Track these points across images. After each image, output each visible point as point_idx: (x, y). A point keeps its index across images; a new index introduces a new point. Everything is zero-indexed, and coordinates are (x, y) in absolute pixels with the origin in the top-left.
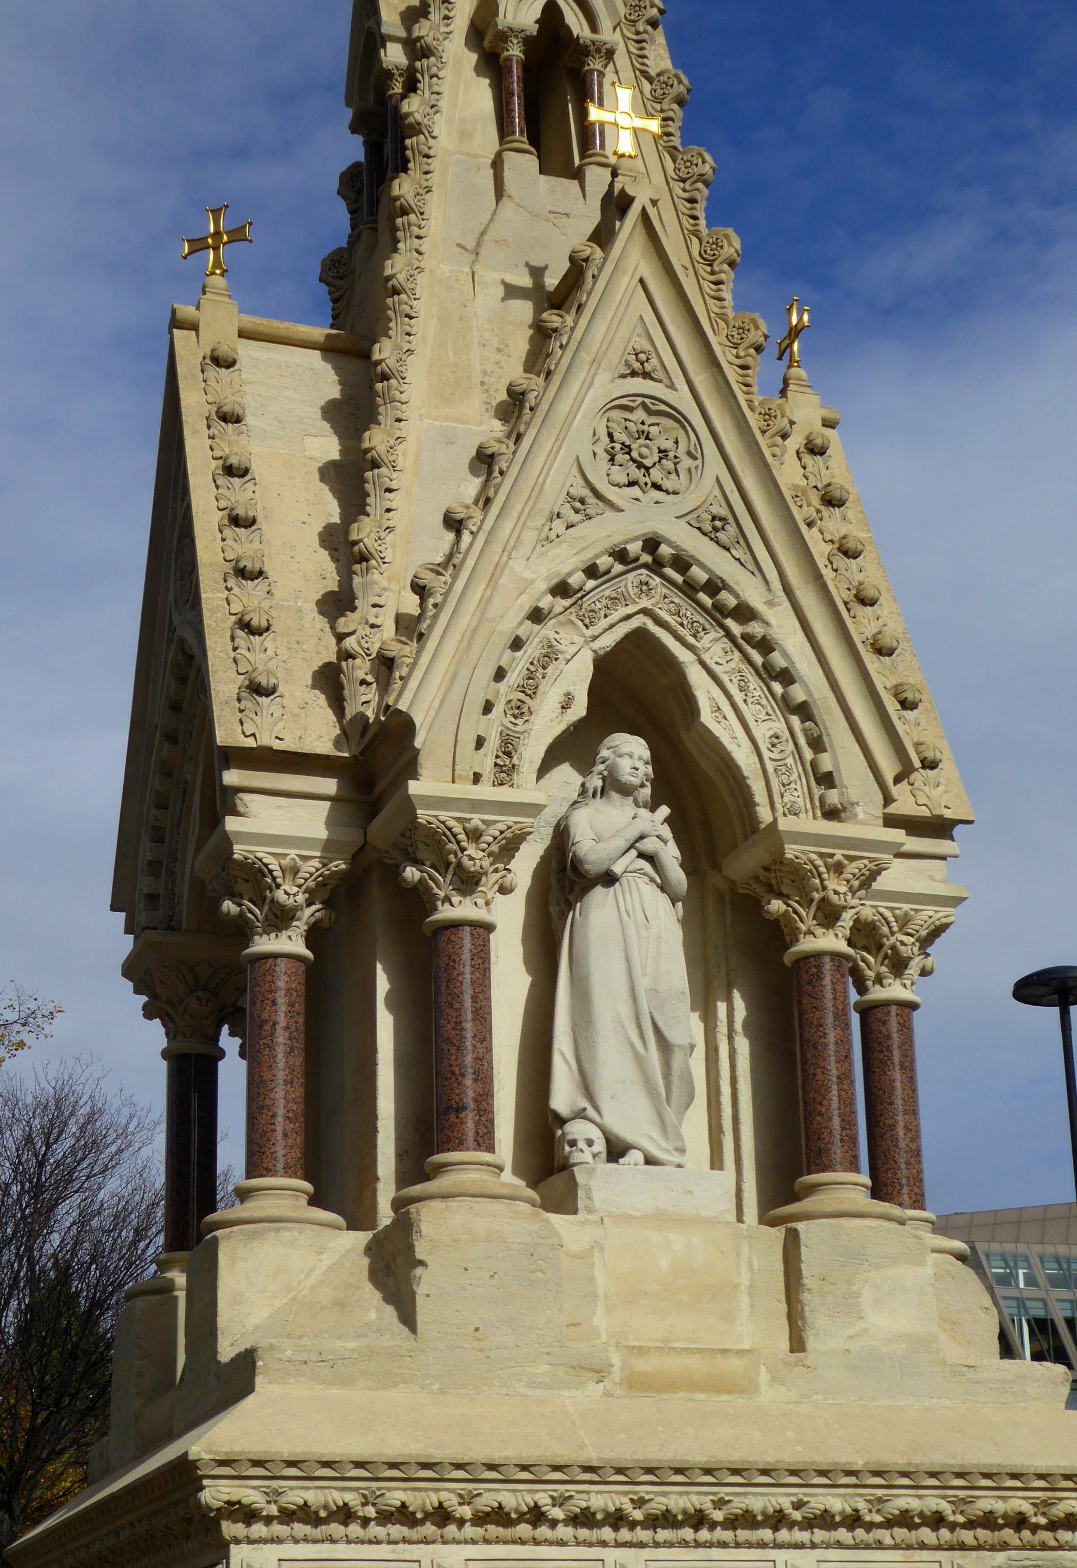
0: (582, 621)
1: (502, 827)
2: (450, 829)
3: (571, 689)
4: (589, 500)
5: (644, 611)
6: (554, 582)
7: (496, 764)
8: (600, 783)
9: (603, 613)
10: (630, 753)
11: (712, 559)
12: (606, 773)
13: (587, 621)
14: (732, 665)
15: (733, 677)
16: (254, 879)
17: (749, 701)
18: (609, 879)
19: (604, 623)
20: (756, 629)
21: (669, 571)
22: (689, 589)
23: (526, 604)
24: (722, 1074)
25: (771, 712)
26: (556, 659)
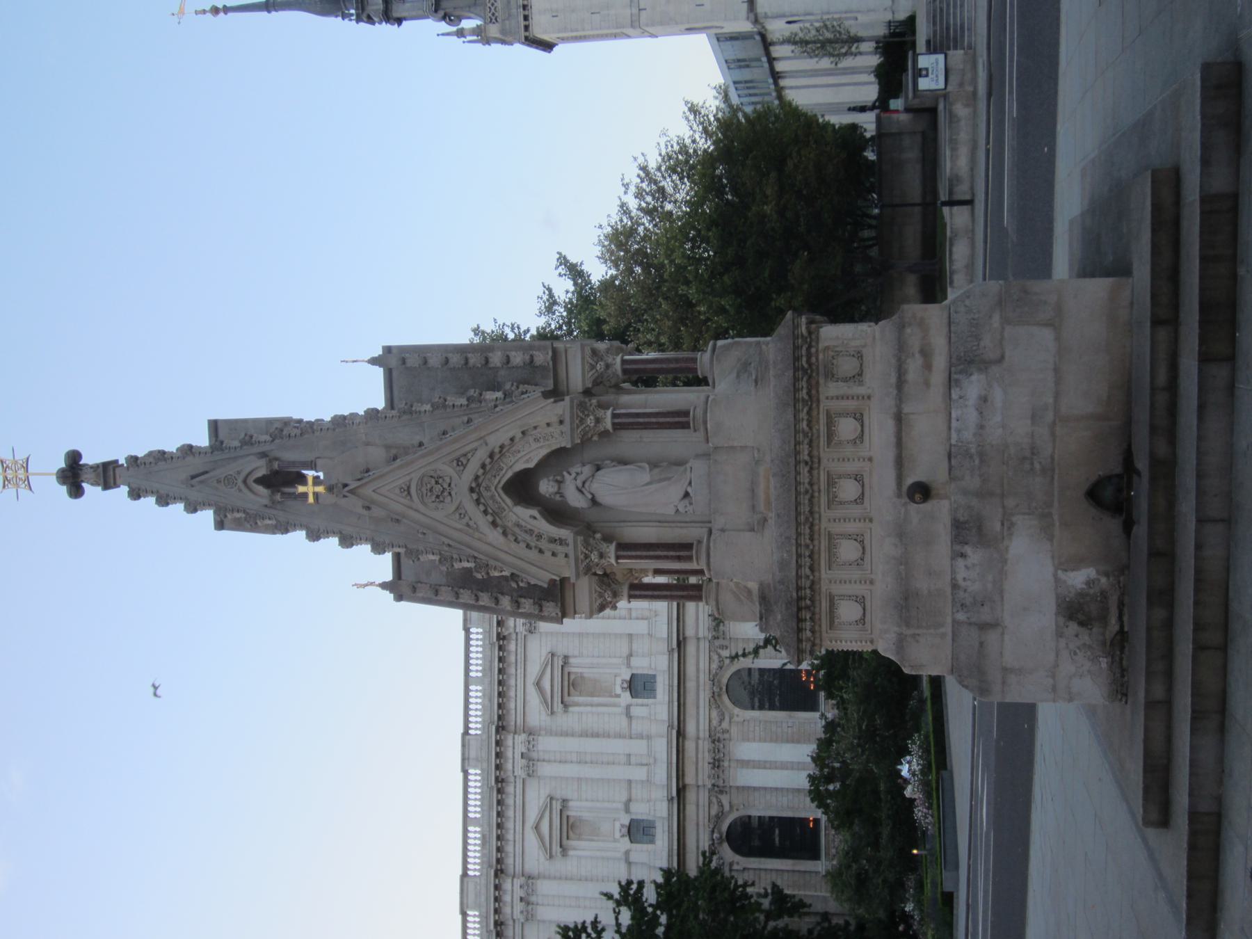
4: (460, 512)
11: (473, 467)
20: (497, 450)
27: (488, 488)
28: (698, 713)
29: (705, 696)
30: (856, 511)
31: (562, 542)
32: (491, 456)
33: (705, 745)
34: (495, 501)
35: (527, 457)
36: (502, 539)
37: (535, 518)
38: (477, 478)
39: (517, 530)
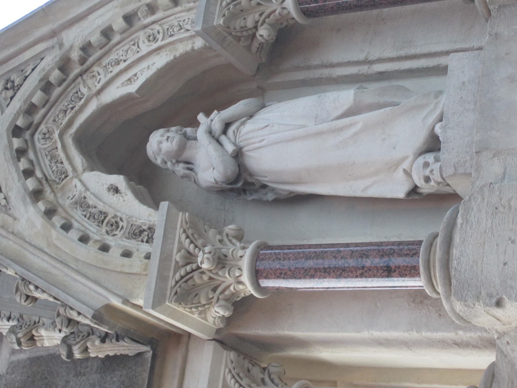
0: (63, 180)
1: (183, 236)
2: (182, 277)
3: (106, 186)
5: (61, 136)
6: (28, 200)
7: (147, 242)
8: (181, 165)
9: (60, 165)
10: (160, 144)
12: (174, 161)
13: (63, 176)
14: (101, 71)
15: (109, 70)
17: (124, 58)
18: (238, 155)
19: (67, 165)
20: (75, 55)
21: (37, 118)
24: (396, 68)
25: (132, 43)
26: (85, 198)
27: (47, 136)
32: (64, 66)
34: (53, 158)
36: (39, 221)
37: (116, 190)
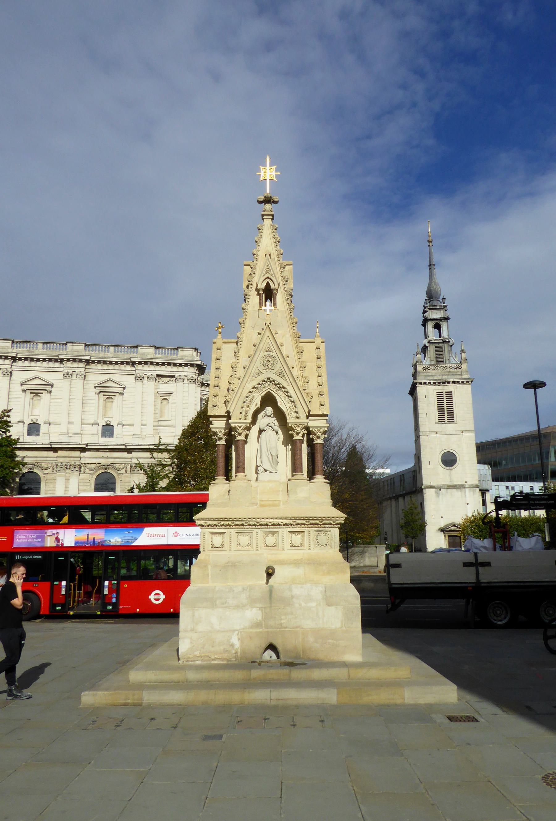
4: (259, 373)
11: (278, 379)
16: (215, 434)
22: (276, 384)
23: (248, 391)
28: (93, 458)
29: (102, 461)
30: (261, 544)
31: (246, 417)
33: (77, 461)
35: (283, 403)
38: (274, 381)
39: (251, 397)
